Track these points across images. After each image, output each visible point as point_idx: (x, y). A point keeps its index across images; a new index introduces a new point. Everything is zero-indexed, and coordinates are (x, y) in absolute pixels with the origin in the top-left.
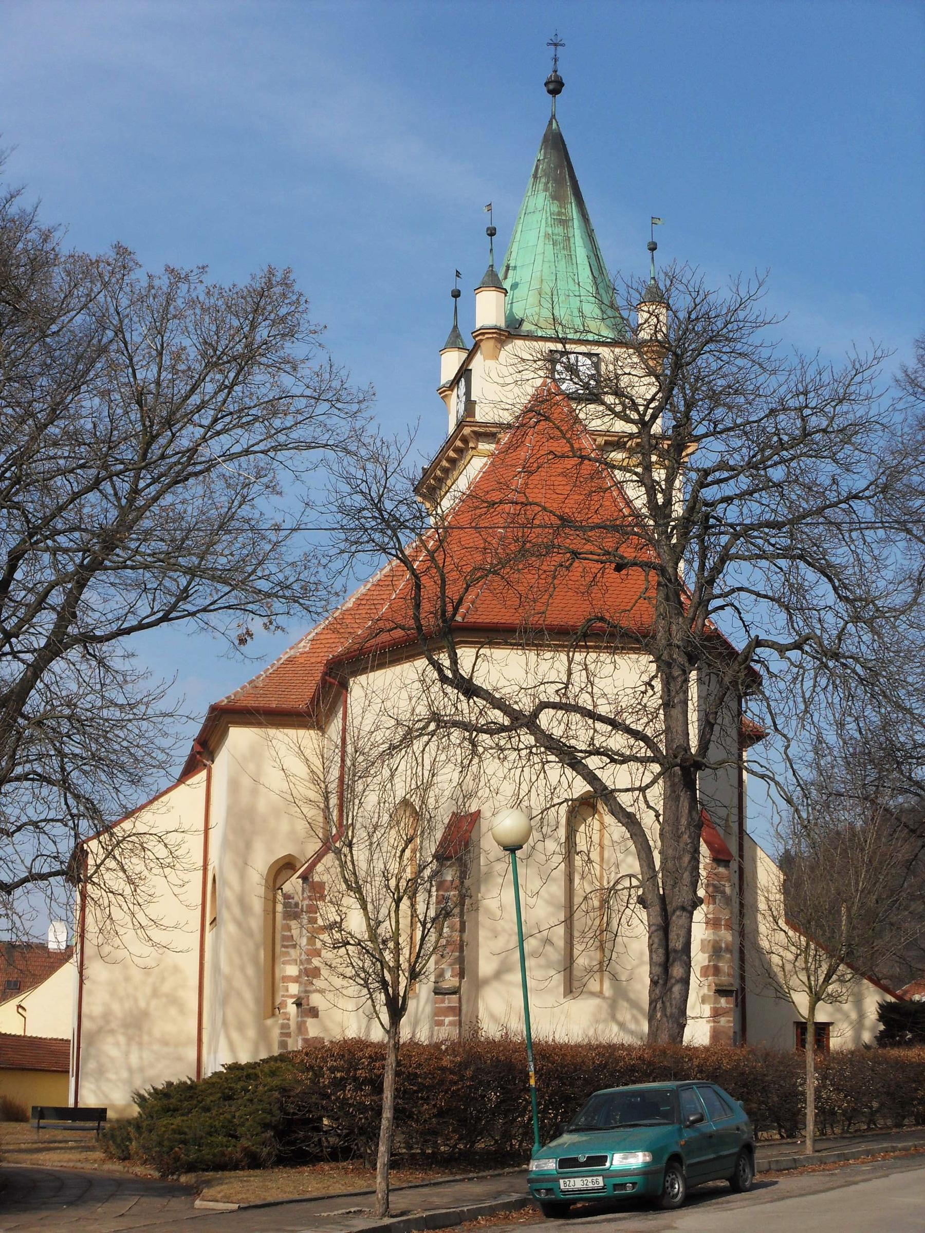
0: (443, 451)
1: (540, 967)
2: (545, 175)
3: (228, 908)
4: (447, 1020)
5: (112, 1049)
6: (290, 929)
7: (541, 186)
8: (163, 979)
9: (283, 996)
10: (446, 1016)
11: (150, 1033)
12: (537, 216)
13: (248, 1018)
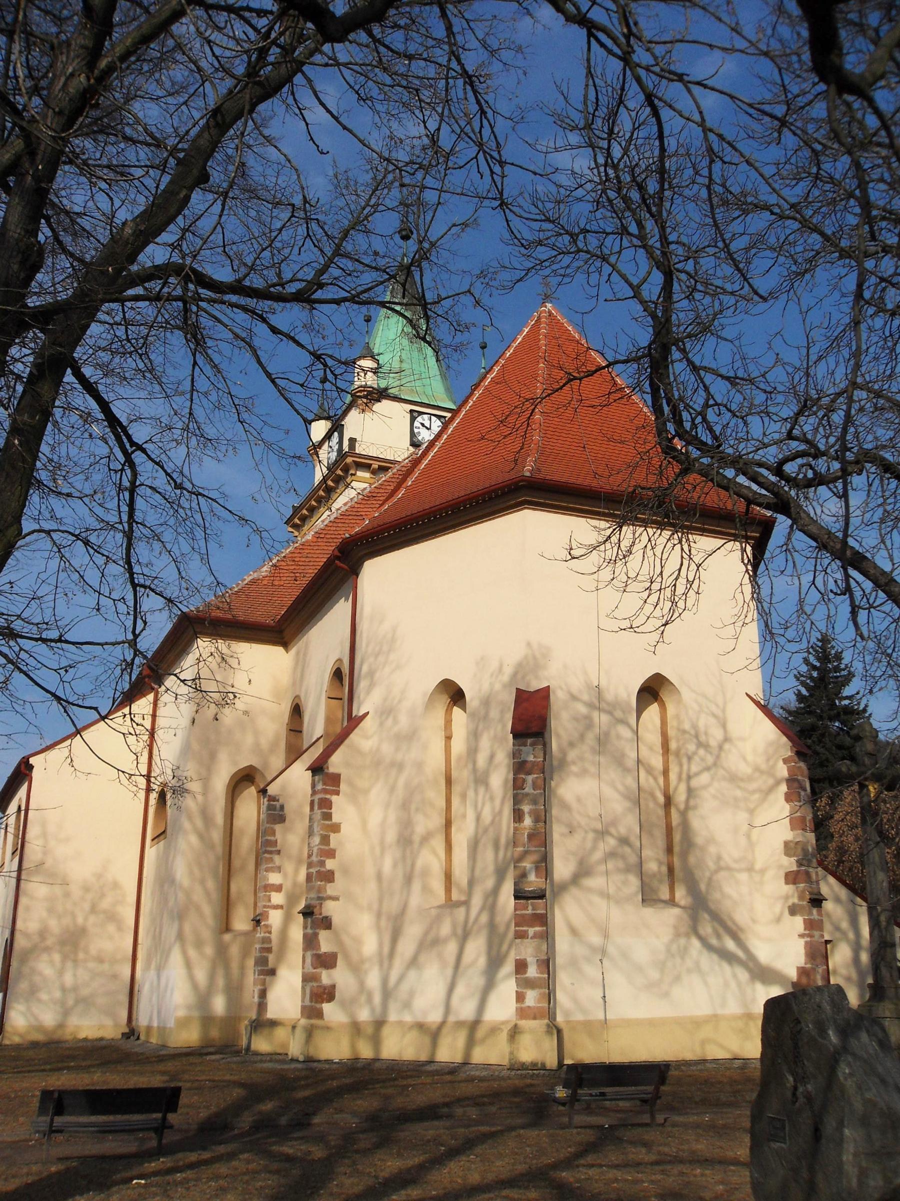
0: (309, 499)
1: (619, 870)
3: (190, 818)
4: (531, 931)
5: (46, 967)
6: (274, 834)
8: (103, 895)
9: (265, 906)
10: (532, 926)
11: (86, 952)
13: (207, 935)
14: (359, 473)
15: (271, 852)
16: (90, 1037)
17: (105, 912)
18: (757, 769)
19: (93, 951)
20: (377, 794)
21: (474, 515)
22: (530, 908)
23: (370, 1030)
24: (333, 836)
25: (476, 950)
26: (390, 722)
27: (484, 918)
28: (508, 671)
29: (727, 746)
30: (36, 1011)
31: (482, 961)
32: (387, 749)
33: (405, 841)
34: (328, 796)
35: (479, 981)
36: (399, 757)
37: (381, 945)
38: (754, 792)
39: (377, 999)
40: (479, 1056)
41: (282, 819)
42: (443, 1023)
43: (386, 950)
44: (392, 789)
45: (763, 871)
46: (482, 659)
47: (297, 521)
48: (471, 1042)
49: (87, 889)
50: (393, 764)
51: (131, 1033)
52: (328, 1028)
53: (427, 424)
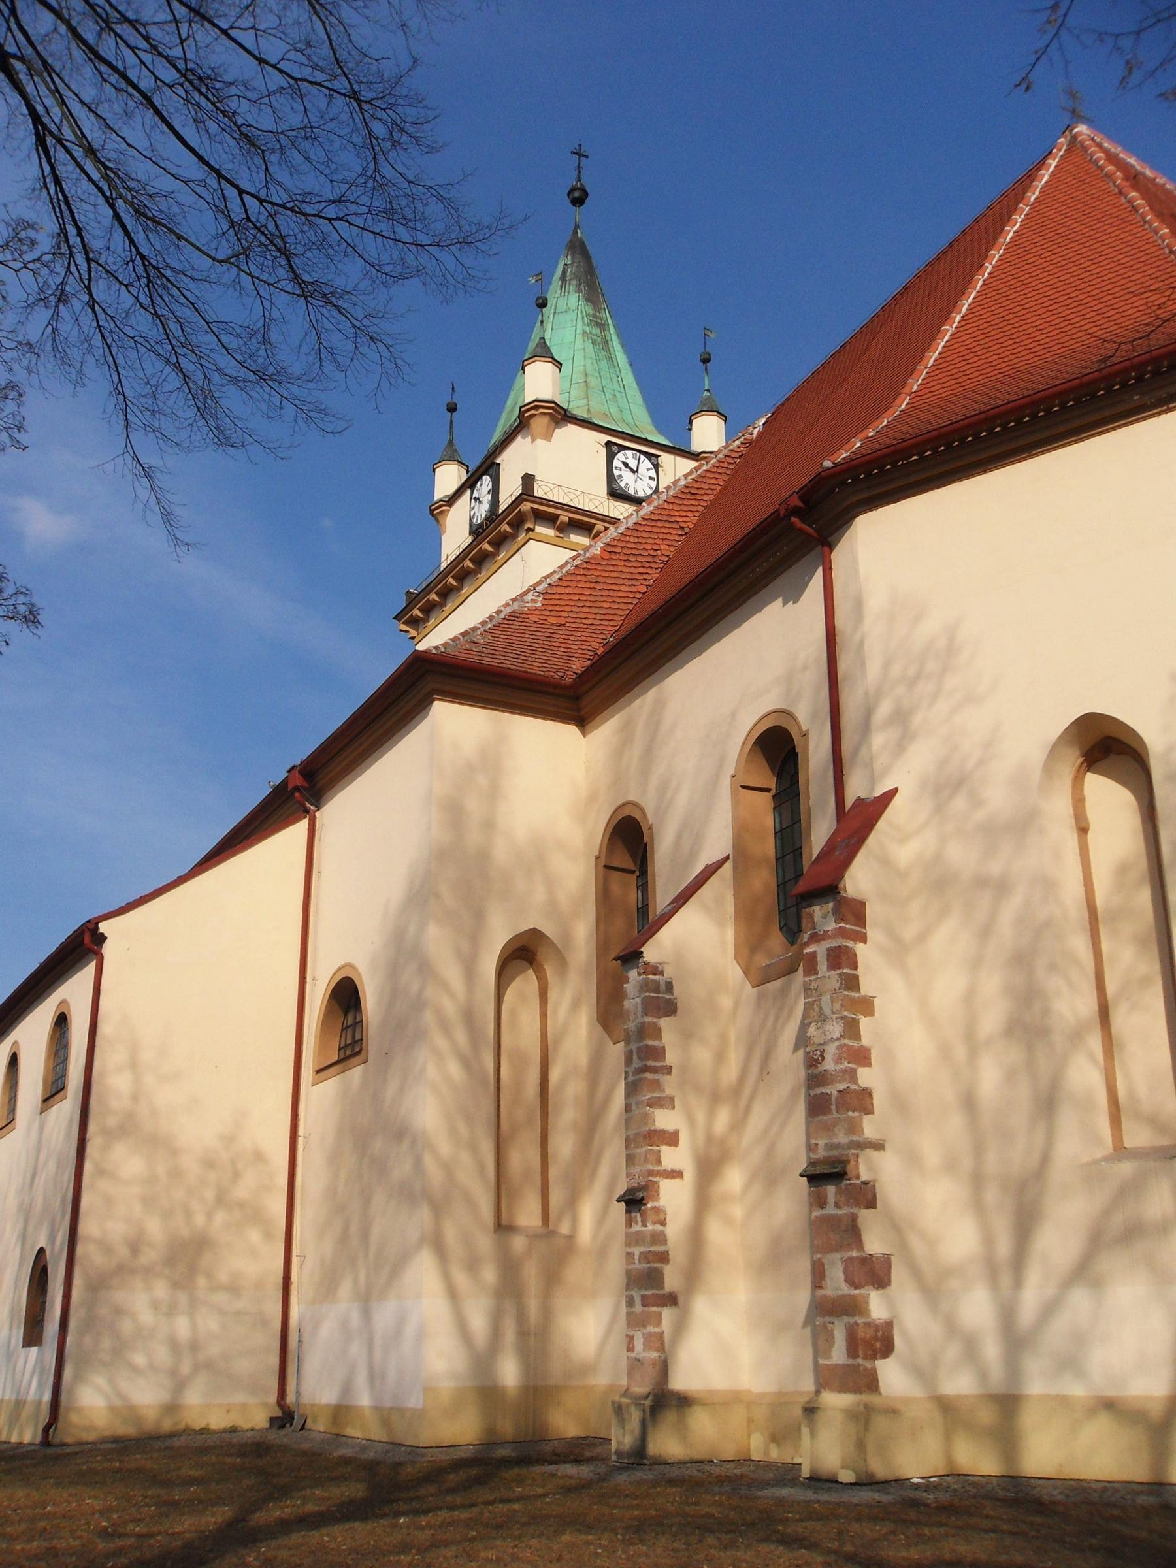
2: (576, 278)
5: (141, 1303)
7: (572, 288)
8: (237, 1175)
11: (209, 1275)
12: (572, 315)
14: (539, 529)
15: (655, 1070)
16: (213, 1427)
17: (241, 1205)
19: (223, 1277)
20: (949, 940)
21: (1096, 416)
23: (986, 1415)
24: (864, 1022)
26: (959, 803)
30: (124, 1385)
32: (962, 856)
33: (1028, 1026)
34: (850, 944)
36: (995, 868)
37: (988, 1240)
39: (992, 1350)
41: (670, 1008)
43: (1004, 1247)
44: (986, 932)
47: (416, 612)
49: (209, 1163)
50: (981, 882)
51: (285, 1417)
52: (892, 1412)
53: (633, 464)
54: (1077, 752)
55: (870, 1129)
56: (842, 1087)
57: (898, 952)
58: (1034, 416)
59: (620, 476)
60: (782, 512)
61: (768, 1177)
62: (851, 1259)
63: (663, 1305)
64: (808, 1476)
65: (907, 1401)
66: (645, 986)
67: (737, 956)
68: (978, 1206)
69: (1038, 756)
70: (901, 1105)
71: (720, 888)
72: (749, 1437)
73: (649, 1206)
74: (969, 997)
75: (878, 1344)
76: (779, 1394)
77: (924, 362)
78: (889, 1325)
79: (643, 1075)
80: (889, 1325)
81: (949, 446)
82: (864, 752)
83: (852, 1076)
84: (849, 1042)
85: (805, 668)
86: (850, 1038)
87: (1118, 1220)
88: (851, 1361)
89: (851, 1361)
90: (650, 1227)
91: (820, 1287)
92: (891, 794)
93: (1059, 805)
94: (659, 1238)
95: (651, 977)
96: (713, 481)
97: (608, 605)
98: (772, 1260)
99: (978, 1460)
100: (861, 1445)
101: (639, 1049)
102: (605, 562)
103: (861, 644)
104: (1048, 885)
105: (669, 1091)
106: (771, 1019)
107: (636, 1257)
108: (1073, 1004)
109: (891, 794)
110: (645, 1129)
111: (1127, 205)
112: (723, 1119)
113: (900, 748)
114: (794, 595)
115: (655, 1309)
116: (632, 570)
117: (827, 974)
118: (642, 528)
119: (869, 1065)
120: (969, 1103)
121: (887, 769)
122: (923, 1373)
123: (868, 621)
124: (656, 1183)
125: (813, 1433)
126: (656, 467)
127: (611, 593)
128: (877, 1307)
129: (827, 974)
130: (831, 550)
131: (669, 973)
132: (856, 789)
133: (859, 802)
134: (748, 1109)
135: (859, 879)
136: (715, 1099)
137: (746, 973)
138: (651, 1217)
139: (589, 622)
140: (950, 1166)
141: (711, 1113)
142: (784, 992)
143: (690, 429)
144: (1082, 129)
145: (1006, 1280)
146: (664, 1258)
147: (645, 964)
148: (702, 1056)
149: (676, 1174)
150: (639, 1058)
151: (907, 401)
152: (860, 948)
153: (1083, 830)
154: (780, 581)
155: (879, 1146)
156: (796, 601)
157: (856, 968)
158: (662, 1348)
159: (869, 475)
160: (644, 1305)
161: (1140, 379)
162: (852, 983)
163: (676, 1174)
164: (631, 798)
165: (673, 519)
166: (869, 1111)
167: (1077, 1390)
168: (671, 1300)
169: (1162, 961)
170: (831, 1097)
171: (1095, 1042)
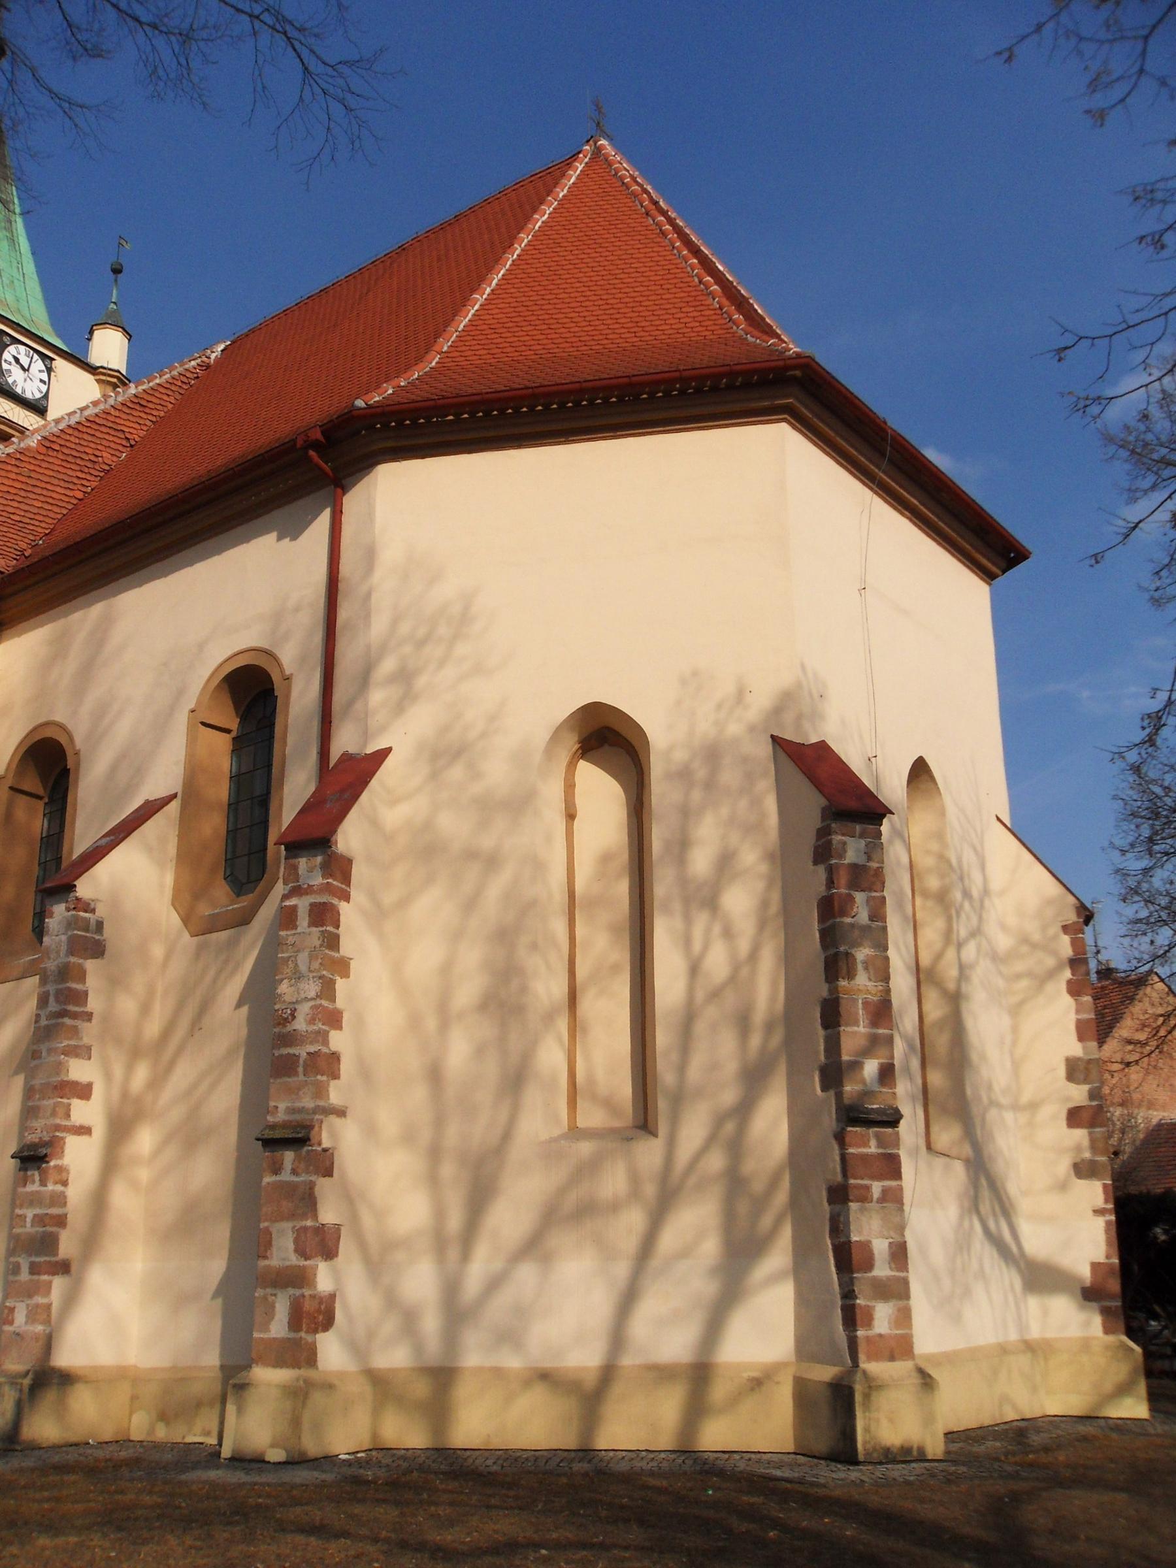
15: (75, 1016)
18: (1025, 940)
20: (432, 908)
21: (738, 407)
22: (873, 1143)
23: (421, 1389)
24: (340, 984)
25: (695, 1225)
26: (456, 773)
27: (716, 1162)
28: (760, 701)
29: (987, 903)
31: (711, 1248)
32: (454, 826)
33: (504, 1002)
34: (335, 901)
35: (706, 1287)
36: (487, 842)
37: (439, 1214)
38: (1018, 977)
39: (431, 1324)
40: (716, 1436)
41: (97, 950)
42: (608, 1373)
43: (455, 1222)
44: (470, 905)
45: (1033, 1106)
46: (695, 674)
48: (696, 1409)
50: (471, 855)
52: (329, 1387)
53: (25, 361)
54: (576, 739)
55: (335, 1095)
56: (312, 1049)
57: (378, 916)
58: (577, 404)
59: (9, 371)
60: (300, 443)
61: (189, 1137)
62: (305, 1229)
63: (54, 1274)
64: (229, 1456)
65: (342, 1375)
66: (71, 924)
67: (175, 902)
68: (433, 1180)
69: (541, 735)
70: (366, 1074)
71: (161, 830)
72: (131, 1415)
73: (52, 1164)
74: (446, 968)
75: (321, 1318)
76: (174, 1368)
77: (454, 324)
78: (332, 1297)
79: (60, 1020)
80: (332, 1297)
81: (487, 414)
82: (359, 706)
83: (323, 1037)
84: (325, 1003)
85: (297, 609)
86: (327, 999)
87: (570, 1201)
88: (292, 1335)
89: (292, 1335)
90: (50, 1187)
91: (265, 1257)
92: (384, 753)
93: (553, 790)
94: (60, 1200)
95: (82, 914)
96: (165, 397)
97: (40, 505)
98: (182, 1228)
99: (406, 1433)
100: (296, 1422)
101: (58, 993)
102: (42, 457)
103: (369, 595)
104: (539, 866)
105: (86, 1040)
106: (212, 973)
107: (29, 1220)
108: (548, 987)
109: (384, 753)
110: (55, 1079)
111: (654, 227)
112: (141, 1074)
113: (400, 708)
114: (293, 531)
115: (45, 1277)
116: (70, 472)
117: (308, 930)
118: (85, 430)
119: (340, 1028)
120: (435, 1075)
121: (383, 729)
122: (358, 1350)
123: (378, 575)
124: (63, 1139)
125: (240, 1411)
126: (49, 370)
127: (45, 492)
128: (324, 1279)
129: (308, 930)
130: (344, 494)
131: (101, 911)
132: (345, 741)
133: (346, 757)
134: (171, 1065)
135: (351, 836)
136: (135, 1053)
137: (186, 921)
138: (53, 1176)
139: (18, 518)
140: (408, 1137)
141: (130, 1069)
142: (232, 944)
143: (89, 340)
144: (603, 142)
145: (453, 1253)
146: (61, 1221)
147: (78, 899)
148: (127, 1006)
149: (84, 1130)
150: (57, 1000)
151: (437, 359)
152: (343, 907)
153: (571, 816)
154: (279, 515)
155: (341, 1113)
156: (294, 537)
157: (338, 927)
158: (47, 1321)
159: (400, 424)
160: (32, 1273)
161: (682, 392)
162: (333, 942)
163: (84, 1130)
164: (58, 718)
165: (119, 428)
166: (336, 1076)
167: (513, 1362)
168: (64, 1268)
169: (632, 950)
170: (285, 1058)
171: (562, 1024)
